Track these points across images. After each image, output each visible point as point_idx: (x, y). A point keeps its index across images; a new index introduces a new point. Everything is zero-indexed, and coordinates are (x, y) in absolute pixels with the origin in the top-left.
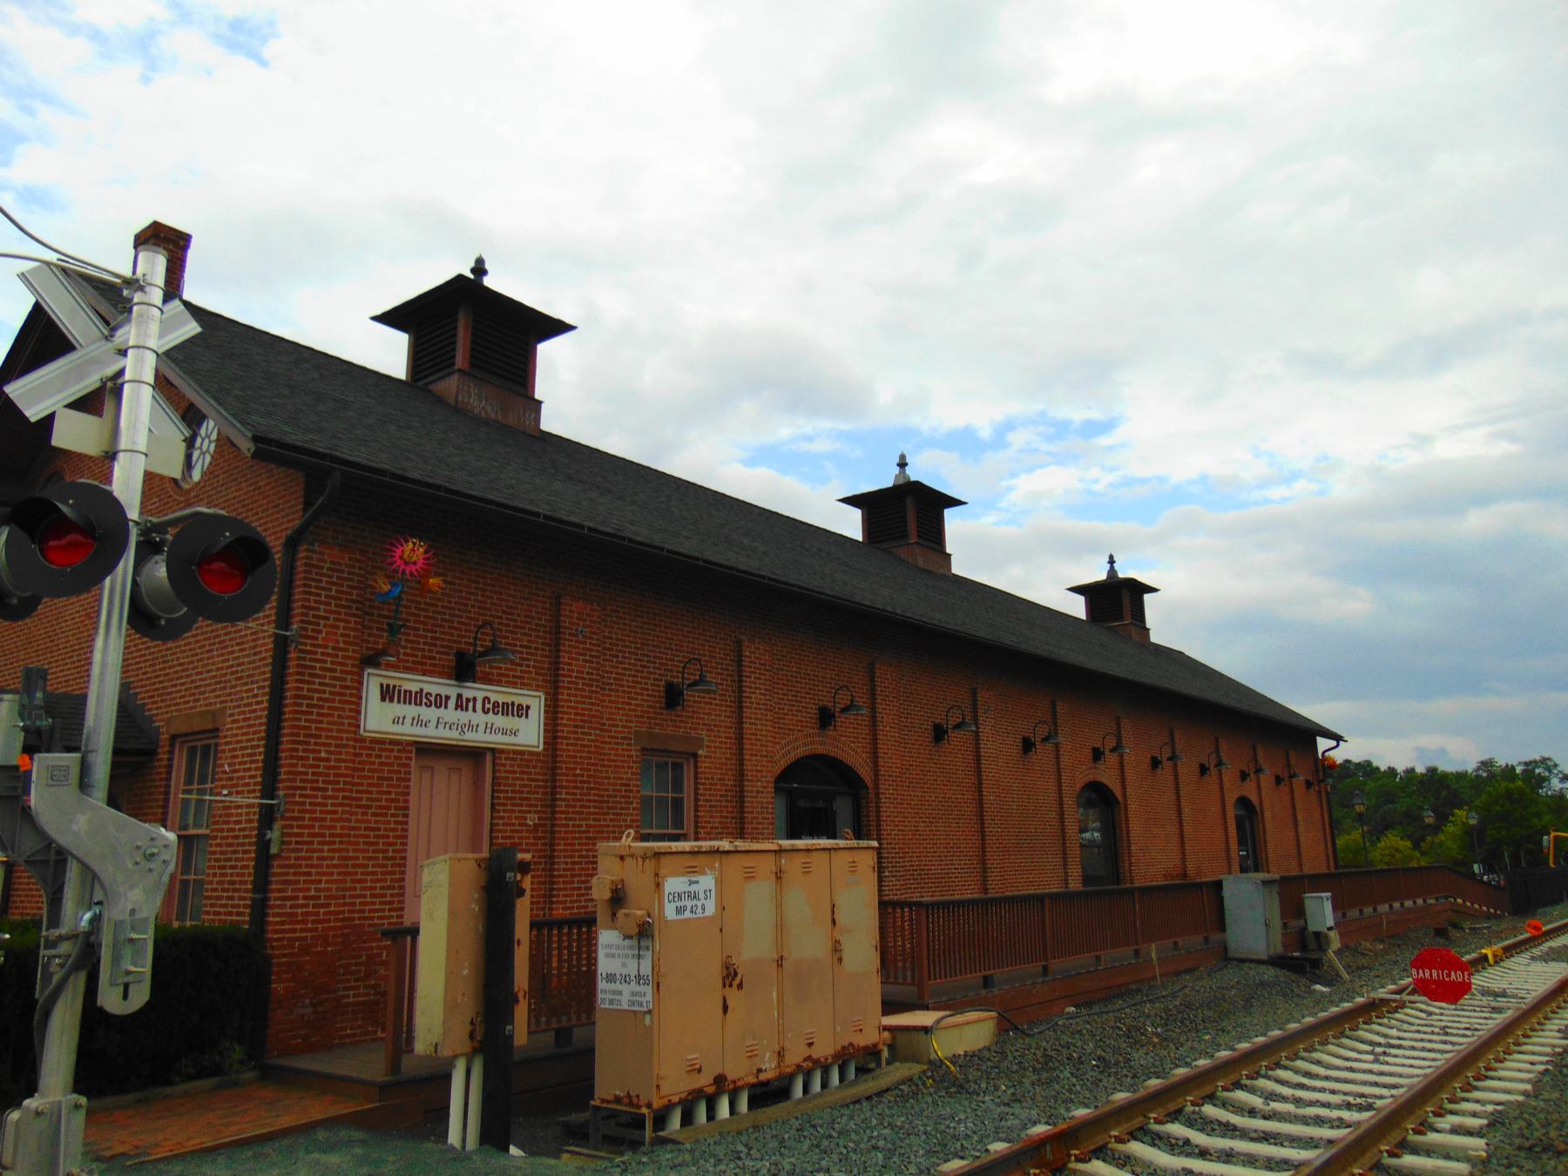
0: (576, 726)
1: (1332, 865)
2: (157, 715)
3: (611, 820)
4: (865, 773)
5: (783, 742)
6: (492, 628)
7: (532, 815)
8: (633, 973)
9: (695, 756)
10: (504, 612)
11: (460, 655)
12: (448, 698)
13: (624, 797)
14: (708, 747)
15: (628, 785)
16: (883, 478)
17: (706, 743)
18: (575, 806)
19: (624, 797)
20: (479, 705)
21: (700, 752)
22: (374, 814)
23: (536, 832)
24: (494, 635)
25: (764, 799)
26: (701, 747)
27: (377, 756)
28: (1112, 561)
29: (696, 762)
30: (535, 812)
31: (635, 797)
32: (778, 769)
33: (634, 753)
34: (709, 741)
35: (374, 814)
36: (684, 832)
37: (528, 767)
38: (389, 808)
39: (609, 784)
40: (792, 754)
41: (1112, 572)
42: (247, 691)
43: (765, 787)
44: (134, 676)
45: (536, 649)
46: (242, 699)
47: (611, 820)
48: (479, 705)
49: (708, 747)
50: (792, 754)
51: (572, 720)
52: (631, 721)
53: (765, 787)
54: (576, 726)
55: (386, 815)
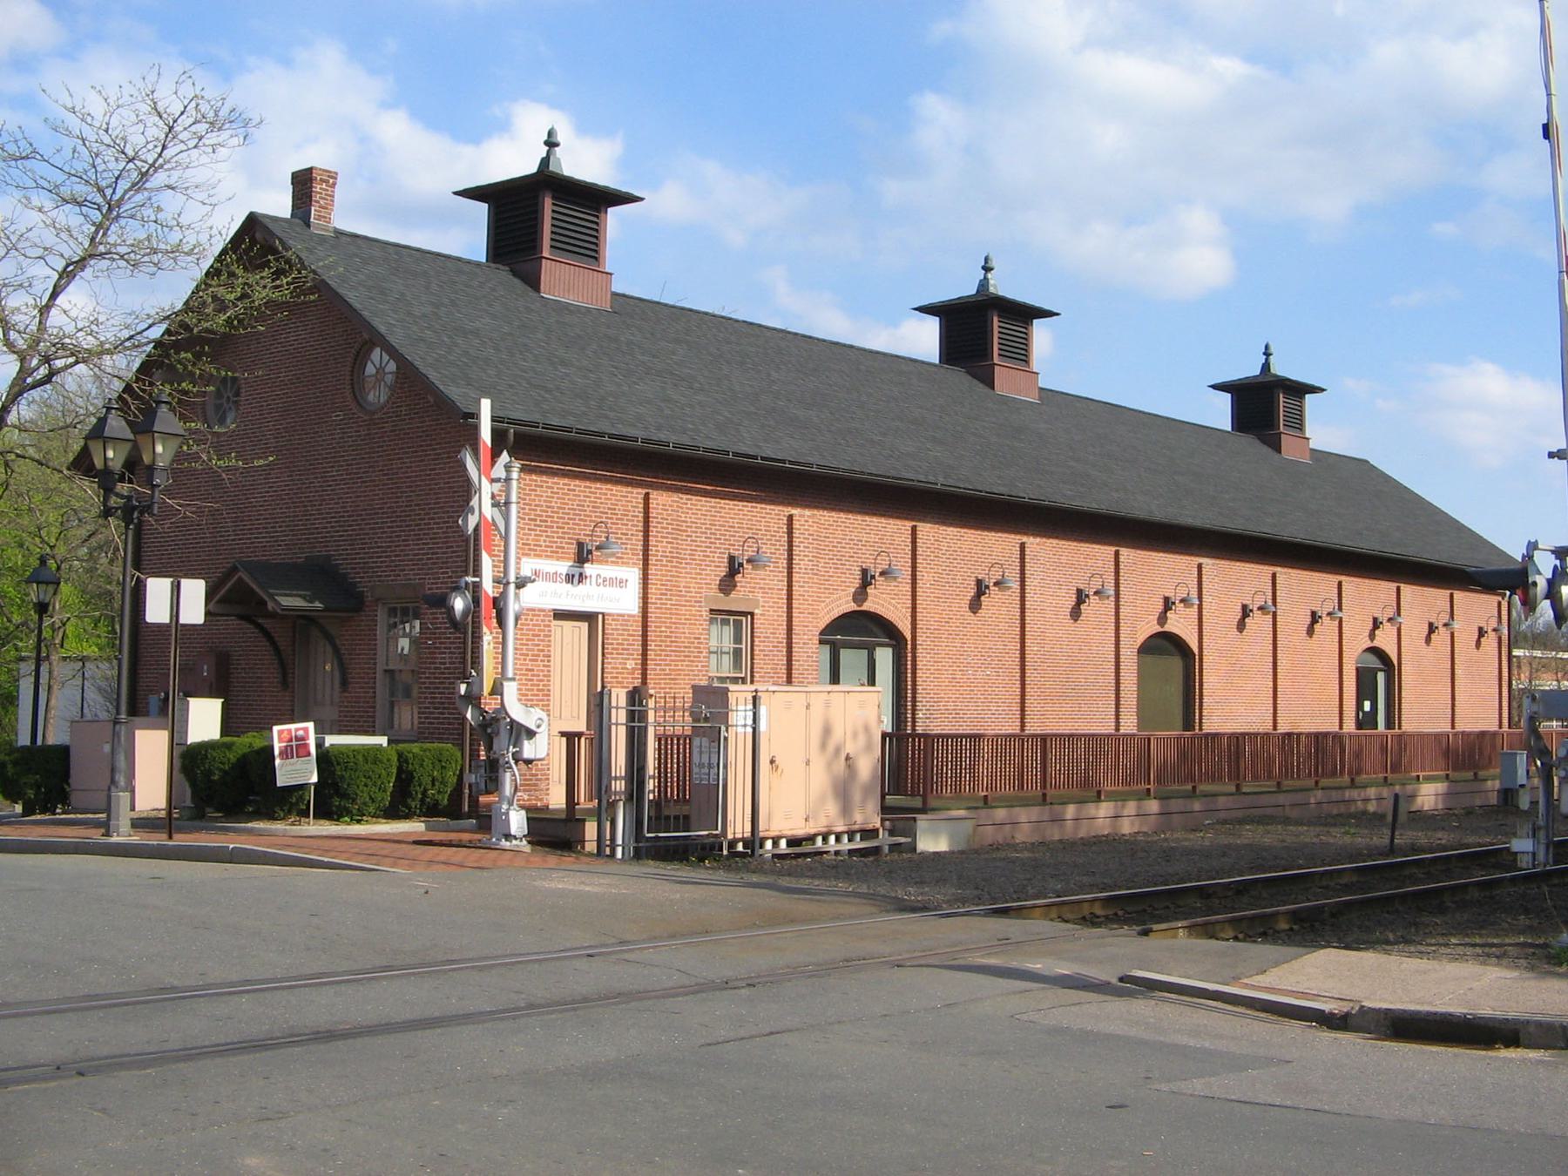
0: (662, 594)
1: (1505, 721)
2: (360, 582)
3: (687, 666)
4: (905, 627)
5: (827, 600)
6: (606, 527)
7: (631, 662)
8: (743, 713)
9: (752, 614)
10: (609, 509)
11: (580, 545)
12: (573, 576)
13: (695, 648)
14: (763, 606)
15: (699, 638)
16: (963, 286)
17: (761, 604)
18: (660, 655)
19: (695, 648)
20: (594, 579)
21: (756, 611)
22: (530, 660)
23: (633, 674)
24: (607, 532)
25: (811, 654)
26: (758, 608)
27: (542, 621)
28: (1267, 354)
29: (752, 619)
30: (633, 659)
31: (704, 648)
32: (822, 625)
33: (704, 613)
34: (765, 602)
35: (530, 660)
36: (743, 675)
37: (627, 625)
38: (539, 656)
39: (685, 638)
40: (836, 611)
41: (1266, 367)
42: (443, 573)
43: (810, 640)
44: (334, 551)
45: (632, 535)
46: (439, 578)
47: (687, 666)
48: (594, 579)
49: (763, 606)
50: (836, 611)
51: (659, 589)
52: (702, 588)
53: (810, 640)
54: (662, 594)
55: (537, 660)
